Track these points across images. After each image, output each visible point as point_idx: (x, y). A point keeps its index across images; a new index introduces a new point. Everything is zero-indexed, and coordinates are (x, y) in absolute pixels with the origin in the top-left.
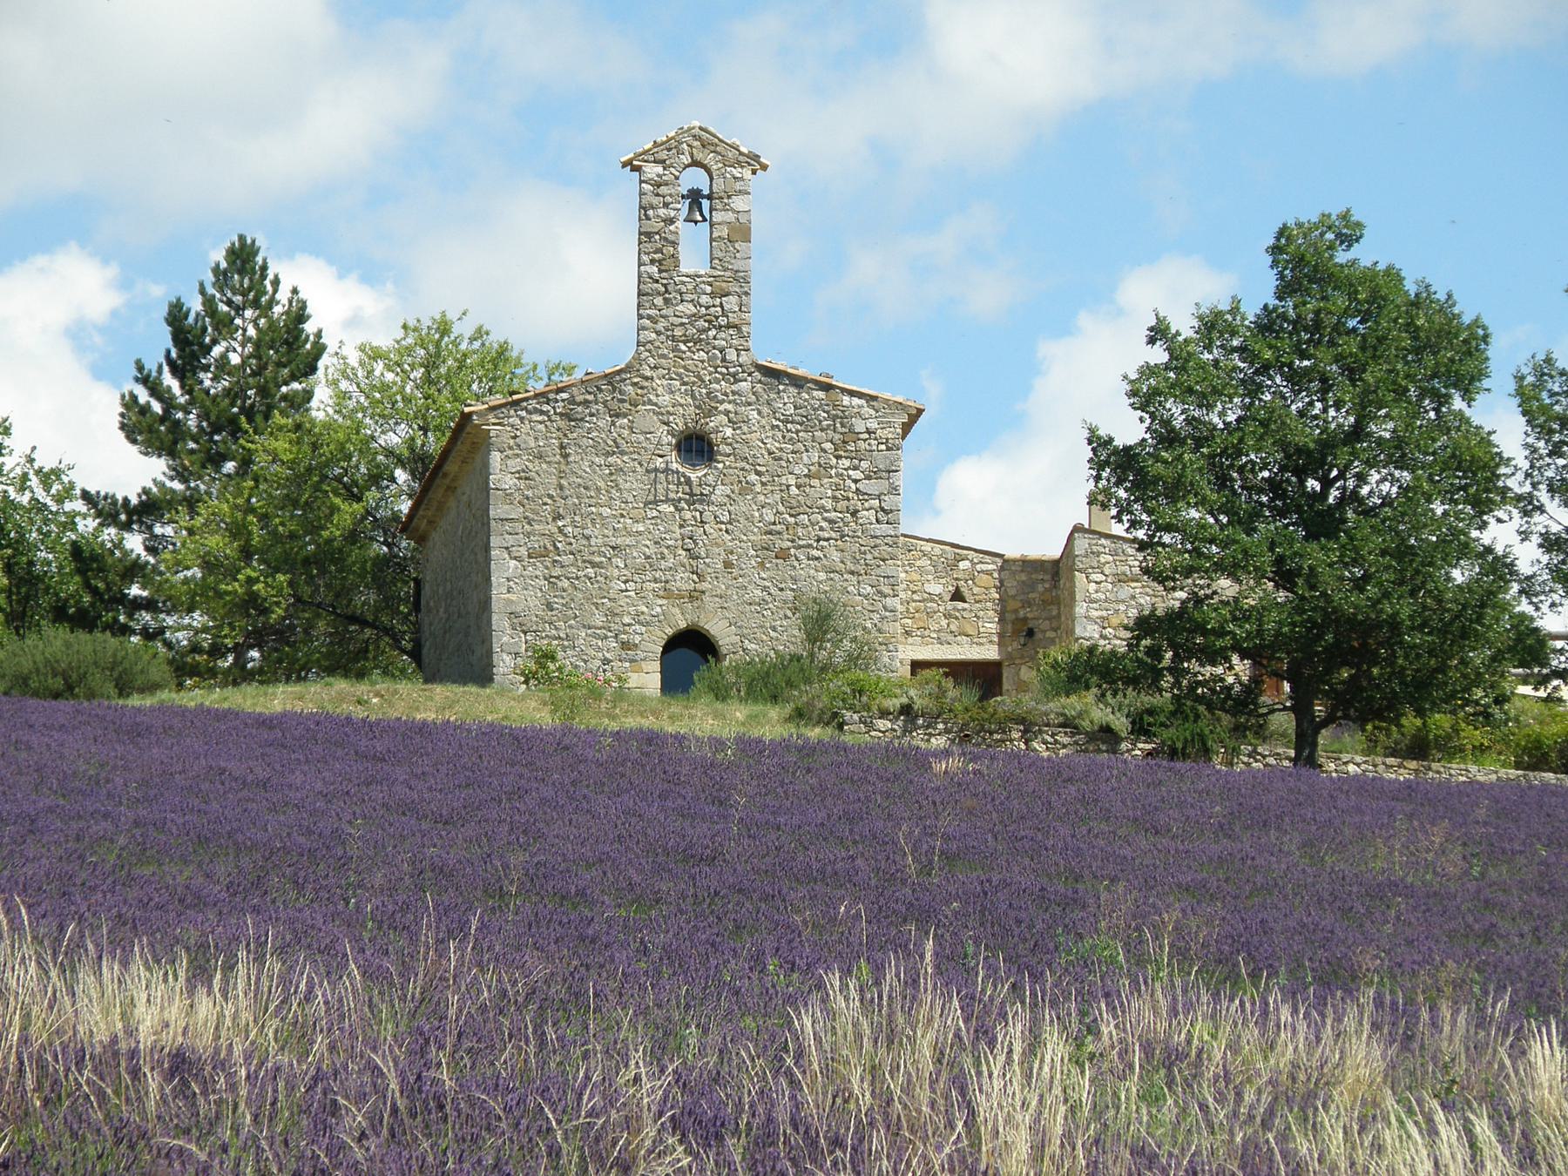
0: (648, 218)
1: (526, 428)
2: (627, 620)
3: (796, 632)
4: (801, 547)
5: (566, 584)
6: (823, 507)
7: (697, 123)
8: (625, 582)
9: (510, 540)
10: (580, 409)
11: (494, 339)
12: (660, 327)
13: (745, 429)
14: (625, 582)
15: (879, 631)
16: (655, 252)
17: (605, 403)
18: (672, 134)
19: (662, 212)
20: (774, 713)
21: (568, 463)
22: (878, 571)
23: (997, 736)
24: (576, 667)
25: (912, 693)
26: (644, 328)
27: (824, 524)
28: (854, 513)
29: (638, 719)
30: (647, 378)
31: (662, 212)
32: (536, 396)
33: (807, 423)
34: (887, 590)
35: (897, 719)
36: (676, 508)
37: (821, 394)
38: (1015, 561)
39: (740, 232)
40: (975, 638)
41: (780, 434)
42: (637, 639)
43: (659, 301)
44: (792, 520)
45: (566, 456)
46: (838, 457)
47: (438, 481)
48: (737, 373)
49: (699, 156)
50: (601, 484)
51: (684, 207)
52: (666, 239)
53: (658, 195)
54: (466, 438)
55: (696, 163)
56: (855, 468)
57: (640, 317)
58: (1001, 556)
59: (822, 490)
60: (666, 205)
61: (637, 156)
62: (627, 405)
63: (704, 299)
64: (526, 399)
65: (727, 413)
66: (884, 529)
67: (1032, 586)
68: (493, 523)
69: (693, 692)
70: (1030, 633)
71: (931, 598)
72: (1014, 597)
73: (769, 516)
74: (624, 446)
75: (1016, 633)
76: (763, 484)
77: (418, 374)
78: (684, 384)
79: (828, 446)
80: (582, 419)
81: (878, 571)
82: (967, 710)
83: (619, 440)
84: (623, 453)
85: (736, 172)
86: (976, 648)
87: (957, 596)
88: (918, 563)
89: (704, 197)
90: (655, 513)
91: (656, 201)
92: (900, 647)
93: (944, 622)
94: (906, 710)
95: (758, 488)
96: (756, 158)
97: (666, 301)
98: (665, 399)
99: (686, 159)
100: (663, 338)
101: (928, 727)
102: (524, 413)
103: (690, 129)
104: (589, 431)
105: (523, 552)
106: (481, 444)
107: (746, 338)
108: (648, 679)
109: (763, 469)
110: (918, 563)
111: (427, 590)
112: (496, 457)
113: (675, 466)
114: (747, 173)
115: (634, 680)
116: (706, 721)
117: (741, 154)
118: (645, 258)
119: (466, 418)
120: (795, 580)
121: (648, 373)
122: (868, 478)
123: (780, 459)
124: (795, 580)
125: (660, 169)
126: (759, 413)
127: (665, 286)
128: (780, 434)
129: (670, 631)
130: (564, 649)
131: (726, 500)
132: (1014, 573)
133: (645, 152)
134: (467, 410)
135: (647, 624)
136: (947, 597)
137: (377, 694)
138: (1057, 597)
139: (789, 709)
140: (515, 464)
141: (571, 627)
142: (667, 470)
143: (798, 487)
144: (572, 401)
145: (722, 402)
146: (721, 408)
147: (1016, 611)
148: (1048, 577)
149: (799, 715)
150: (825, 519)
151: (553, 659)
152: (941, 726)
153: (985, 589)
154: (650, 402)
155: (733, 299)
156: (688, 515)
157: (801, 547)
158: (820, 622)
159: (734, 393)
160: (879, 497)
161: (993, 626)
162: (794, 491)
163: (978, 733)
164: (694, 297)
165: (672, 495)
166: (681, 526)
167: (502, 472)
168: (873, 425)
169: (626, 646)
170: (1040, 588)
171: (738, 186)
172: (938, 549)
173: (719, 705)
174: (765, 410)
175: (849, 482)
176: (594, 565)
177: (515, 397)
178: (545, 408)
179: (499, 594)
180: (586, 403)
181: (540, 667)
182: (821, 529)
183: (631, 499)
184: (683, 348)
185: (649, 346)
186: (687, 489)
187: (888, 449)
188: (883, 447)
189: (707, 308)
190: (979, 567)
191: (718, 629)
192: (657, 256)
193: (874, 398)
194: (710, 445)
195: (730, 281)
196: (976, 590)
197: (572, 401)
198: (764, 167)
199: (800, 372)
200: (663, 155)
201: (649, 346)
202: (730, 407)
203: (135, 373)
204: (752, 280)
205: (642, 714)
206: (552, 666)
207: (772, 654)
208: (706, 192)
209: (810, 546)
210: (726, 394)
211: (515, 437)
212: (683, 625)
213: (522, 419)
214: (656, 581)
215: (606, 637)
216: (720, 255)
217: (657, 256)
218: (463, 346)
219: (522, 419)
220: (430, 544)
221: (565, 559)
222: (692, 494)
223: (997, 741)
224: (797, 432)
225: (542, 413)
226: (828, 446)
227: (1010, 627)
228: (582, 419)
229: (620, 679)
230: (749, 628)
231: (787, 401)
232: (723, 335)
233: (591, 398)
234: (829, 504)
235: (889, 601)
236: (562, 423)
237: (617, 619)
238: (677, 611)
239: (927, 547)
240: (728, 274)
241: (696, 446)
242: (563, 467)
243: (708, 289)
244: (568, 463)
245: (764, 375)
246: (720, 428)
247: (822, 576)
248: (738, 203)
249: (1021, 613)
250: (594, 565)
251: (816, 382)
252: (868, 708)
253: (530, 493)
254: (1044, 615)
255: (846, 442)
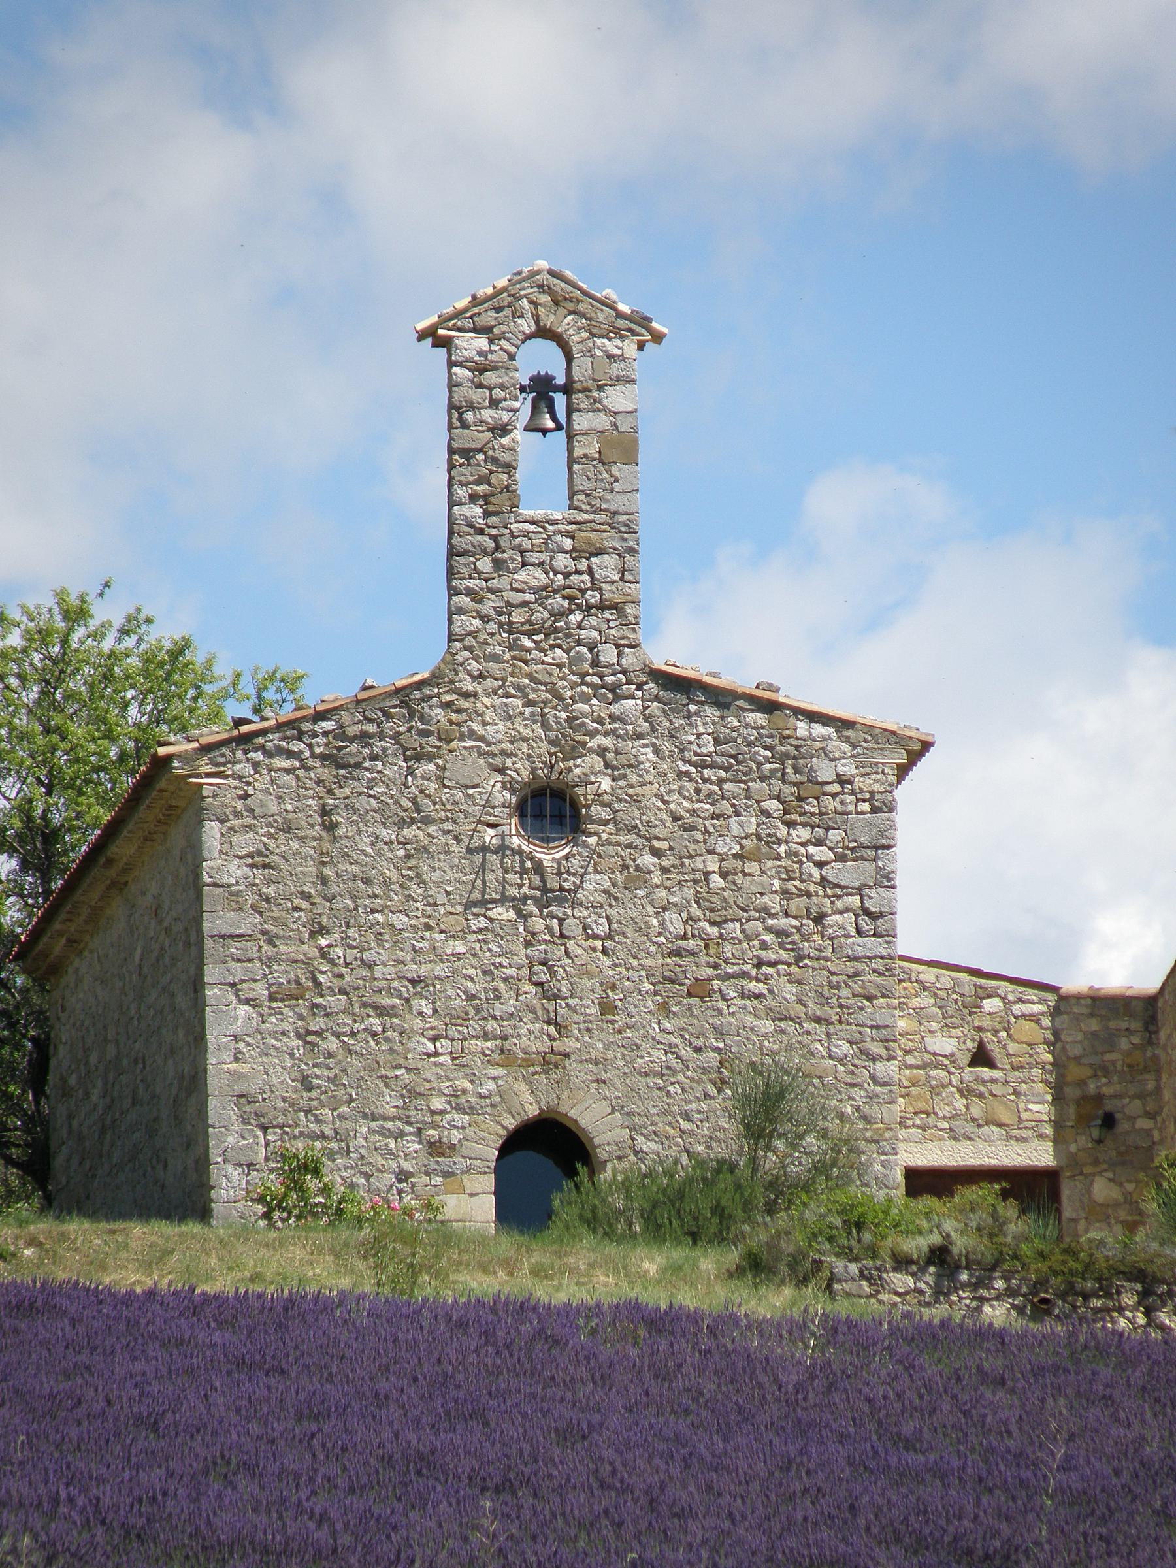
0: (465, 425)
1: (262, 782)
2: (437, 1103)
3: (724, 1122)
4: (729, 976)
5: (332, 1044)
6: (765, 909)
7: (543, 264)
8: (434, 1039)
9: (238, 971)
10: (354, 747)
11: (163, 634)
12: (488, 607)
13: (633, 778)
14: (434, 1039)
15: (864, 1118)
16: (478, 482)
17: (396, 736)
18: (502, 282)
19: (488, 414)
20: (709, 1262)
21: (335, 839)
22: (861, 1017)
23: (1096, 1303)
24: (352, 1186)
25: (949, 1225)
26: (461, 611)
27: (768, 938)
28: (819, 919)
29: (481, 1277)
30: (466, 695)
31: (488, 414)
32: (279, 727)
33: (737, 767)
34: (876, 1049)
35: (923, 1270)
36: (519, 913)
37: (759, 718)
38: (1078, 997)
39: (621, 447)
40: (1014, 1130)
41: (691, 787)
42: (456, 1136)
43: (485, 564)
44: (714, 931)
45: (331, 827)
46: (790, 824)
47: (95, 872)
48: (617, 685)
49: (549, 320)
50: (392, 874)
51: (524, 406)
52: (495, 460)
53: (480, 386)
54: (157, 799)
55: (543, 332)
56: (819, 843)
57: (453, 592)
58: (1054, 989)
59: (763, 880)
60: (494, 403)
61: (444, 320)
62: (433, 740)
63: (562, 561)
64: (263, 732)
65: (602, 751)
66: (871, 945)
67: (1109, 1040)
68: (208, 943)
69: (556, 1228)
70: (1109, 1121)
71: (935, 1061)
72: (1077, 1059)
73: (675, 924)
74: (429, 809)
75: (1083, 1120)
76: (664, 870)
77: (31, 695)
78: (530, 703)
79: (773, 805)
80: (358, 765)
81: (861, 1017)
82: (1041, 1255)
83: (422, 800)
84: (427, 821)
85: (612, 346)
86: (1018, 1148)
87: (981, 1057)
88: (915, 1002)
89: (557, 389)
90: (483, 922)
91: (477, 396)
92: (901, 1146)
93: (960, 1103)
94: (939, 1256)
95: (656, 878)
96: (645, 322)
97: (498, 565)
98: (498, 730)
99: (526, 325)
100: (492, 627)
101: (976, 1286)
102: (258, 756)
103: (533, 274)
104: (371, 784)
105: (260, 990)
106: (187, 808)
107: (633, 625)
108: (474, 1205)
109: (663, 845)
110: (915, 1002)
111: (61, 1059)
112: (212, 831)
113: (515, 841)
114: (629, 348)
115: (453, 1206)
116: (583, 1275)
117: (620, 315)
118: (461, 492)
119: (162, 764)
120: (719, 1032)
121: (468, 686)
122: (841, 858)
123: (693, 828)
124: (719, 1032)
125: (482, 342)
126: (656, 751)
127: (494, 538)
128: (691, 787)
129: (511, 1123)
130: (331, 1155)
131: (602, 898)
132: (1077, 1018)
133: (458, 314)
134: (162, 751)
135: (472, 1110)
136: (964, 1059)
137: (32, 1242)
138: (1155, 1059)
139: (733, 1256)
140: (244, 842)
141: (342, 1117)
142: (502, 849)
143: (724, 875)
144: (340, 734)
145: (592, 734)
146: (592, 744)
147: (1082, 1083)
148: (1136, 1025)
149: (757, 1267)
150: (770, 930)
151: (316, 1172)
152: (999, 1284)
153: (1028, 1041)
154: (472, 735)
155: (610, 560)
156: (538, 924)
157: (729, 976)
158: (766, 1109)
159: (613, 718)
160: (859, 891)
161: (1044, 1108)
162: (717, 881)
163: (1063, 1296)
164: (545, 556)
165: (512, 891)
166: (528, 944)
167: (223, 856)
168: (847, 768)
169: (436, 1148)
170: (1124, 1044)
171: (616, 369)
172: (947, 978)
173: (611, 1249)
174: (666, 746)
175: (809, 867)
176: (380, 1011)
177: (244, 729)
178: (296, 746)
179: (220, 1065)
180: (364, 737)
181: (295, 1191)
182: (764, 946)
183: (441, 899)
184: (528, 643)
185: (469, 641)
186: (536, 880)
187: (875, 810)
188: (865, 807)
189: (567, 575)
190: (1017, 1009)
191: (591, 1115)
192: (482, 489)
193: (848, 724)
194: (575, 806)
195: (602, 531)
196: (1012, 1047)
197: (340, 734)
198: (658, 338)
199: (724, 682)
200: (489, 318)
201: (469, 641)
202: (607, 742)
203: (271, 671)
204: (641, 528)
205: (484, 1268)
206: (312, 1184)
207: (684, 1158)
208: (560, 380)
209: (745, 975)
210: (600, 721)
211: (246, 796)
212: (532, 1111)
213: (256, 765)
214: (486, 1036)
215: (401, 1134)
216: (587, 485)
217: (482, 489)
218: (107, 644)
219: (256, 765)
220: (69, 978)
221: (329, 1001)
222: (545, 890)
223: (1097, 1310)
224: (720, 782)
225: (290, 754)
226: (773, 805)
227: (1072, 1111)
228: (358, 765)
229: (428, 1206)
230: (646, 1110)
231: (702, 728)
232: (594, 621)
233: (371, 728)
234: (774, 903)
235: (880, 1068)
236: (325, 773)
237: (421, 1102)
238: (521, 1087)
239: (929, 975)
240: (601, 518)
241: (551, 808)
242: (326, 846)
243: (568, 543)
244: (335, 839)
245: (664, 687)
246: (591, 776)
247: (766, 1026)
248: (616, 398)
249: (1092, 1087)
250: (380, 1011)
251: (750, 698)
252: (873, 1252)
253: (270, 891)
254: (1132, 1089)
255: (803, 796)
